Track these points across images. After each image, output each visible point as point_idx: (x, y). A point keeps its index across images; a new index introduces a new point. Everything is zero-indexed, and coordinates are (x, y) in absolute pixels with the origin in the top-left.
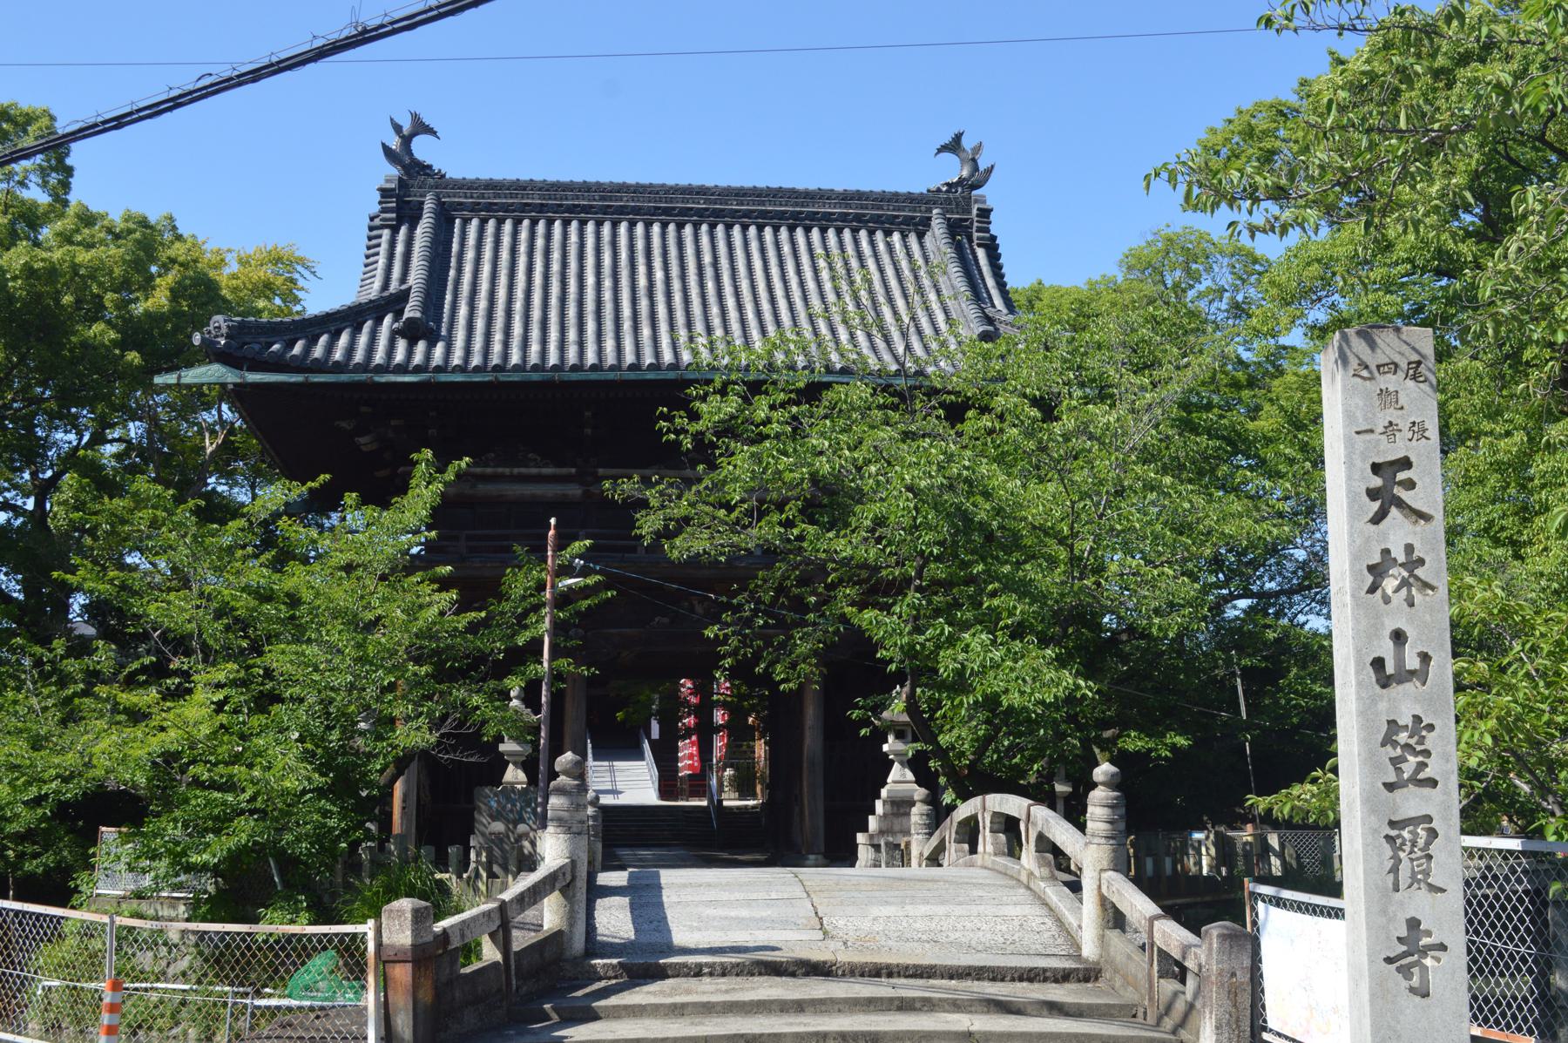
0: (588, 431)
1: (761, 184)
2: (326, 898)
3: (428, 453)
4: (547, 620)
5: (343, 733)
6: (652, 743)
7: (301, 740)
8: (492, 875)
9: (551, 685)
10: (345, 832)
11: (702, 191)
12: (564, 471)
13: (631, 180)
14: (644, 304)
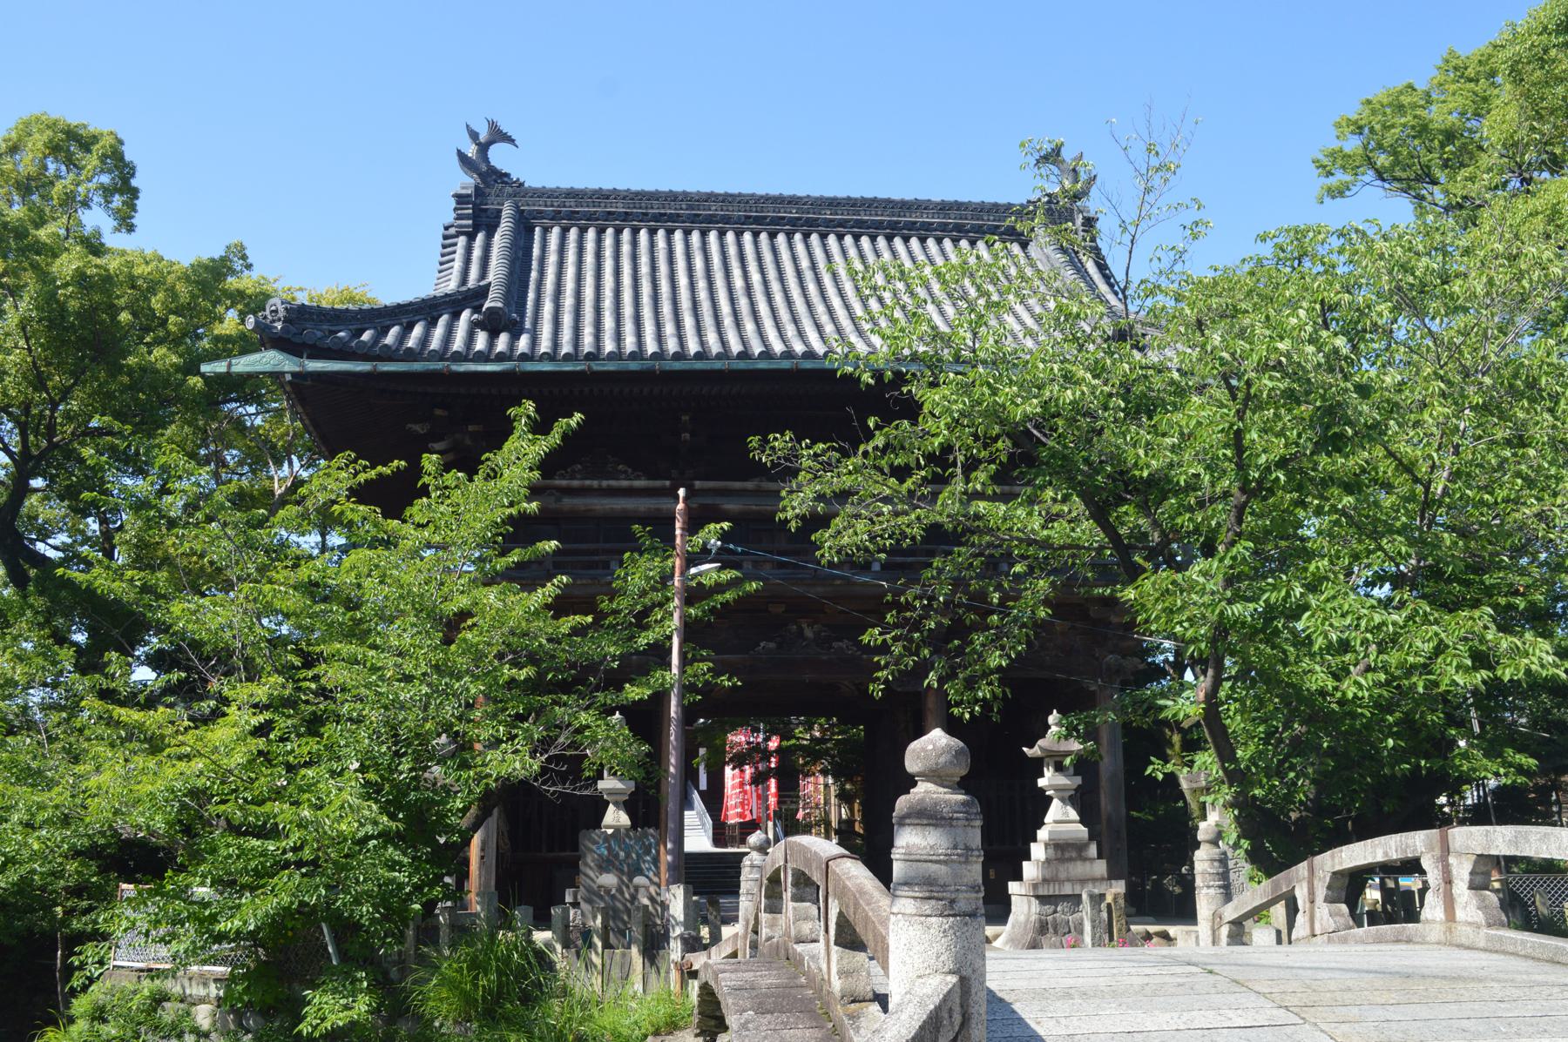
0: (686, 436)
1: (855, 194)
2: (394, 972)
3: (529, 407)
4: (676, 615)
5: (415, 760)
6: (700, 793)
7: (363, 769)
8: (607, 945)
9: (681, 697)
10: (417, 888)
11: (793, 201)
12: (658, 483)
13: (720, 190)
14: (743, 303)
